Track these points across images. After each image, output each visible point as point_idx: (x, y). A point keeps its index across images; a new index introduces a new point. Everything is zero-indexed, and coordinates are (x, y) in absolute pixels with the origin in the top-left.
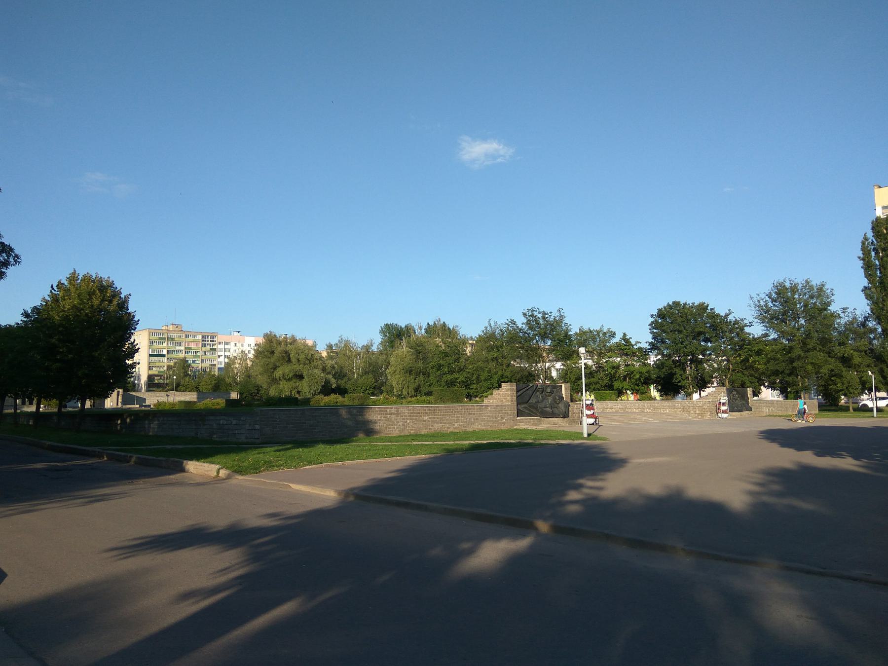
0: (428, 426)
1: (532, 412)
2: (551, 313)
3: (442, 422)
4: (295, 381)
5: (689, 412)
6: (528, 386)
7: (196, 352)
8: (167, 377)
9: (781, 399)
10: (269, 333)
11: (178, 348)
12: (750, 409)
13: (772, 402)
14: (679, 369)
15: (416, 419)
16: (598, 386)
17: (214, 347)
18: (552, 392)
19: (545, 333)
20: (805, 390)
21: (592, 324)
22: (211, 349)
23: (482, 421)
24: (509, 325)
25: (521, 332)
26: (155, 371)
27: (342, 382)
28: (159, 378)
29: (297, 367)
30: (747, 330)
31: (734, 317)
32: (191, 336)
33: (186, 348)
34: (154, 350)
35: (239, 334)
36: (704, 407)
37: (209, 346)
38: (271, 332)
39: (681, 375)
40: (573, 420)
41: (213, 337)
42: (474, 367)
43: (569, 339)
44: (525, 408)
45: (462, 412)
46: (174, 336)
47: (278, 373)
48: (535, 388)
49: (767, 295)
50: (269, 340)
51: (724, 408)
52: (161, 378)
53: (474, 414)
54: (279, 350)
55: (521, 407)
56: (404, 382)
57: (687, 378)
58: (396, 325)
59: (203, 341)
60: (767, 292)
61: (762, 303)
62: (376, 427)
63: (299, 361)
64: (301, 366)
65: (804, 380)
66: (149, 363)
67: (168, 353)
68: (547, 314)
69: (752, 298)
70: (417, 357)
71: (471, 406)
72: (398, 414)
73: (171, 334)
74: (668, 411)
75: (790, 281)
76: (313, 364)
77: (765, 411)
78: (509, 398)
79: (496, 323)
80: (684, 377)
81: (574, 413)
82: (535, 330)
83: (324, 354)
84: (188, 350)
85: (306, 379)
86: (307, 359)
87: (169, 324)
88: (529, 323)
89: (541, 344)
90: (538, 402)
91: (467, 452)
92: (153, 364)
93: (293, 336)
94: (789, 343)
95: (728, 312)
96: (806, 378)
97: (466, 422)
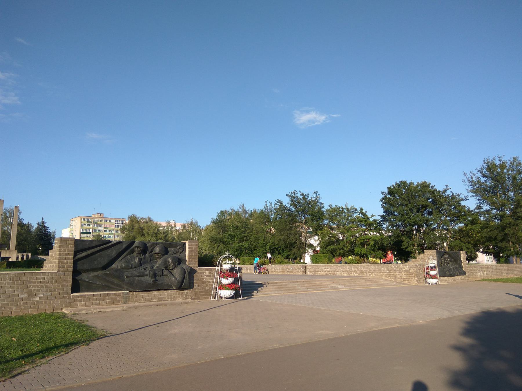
1: (112, 283)
2: (308, 194)
5: (396, 276)
9: (494, 262)
11: (100, 228)
12: (464, 273)
13: (487, 266)
14: (406, 237)
16: (342, 251)
20: (517, 254)
21: (340, 203)
30: (463, 203)
31: (451, 192)
33: (104, 228)
34: (84, 229)
36: (411, 271)
38: (133, 215)
39: (408, 242)
40: (202, 292)
46: (97, 221)
49: (479, 171)
51: (432, 273)
54: (137, 226)
57: (413, 245)
59: (116, 224)
60: (479, 168)
61: (475, 179)
63: (148, 234)
65: (516, 246)
66: (80, 237)
67: (93, 231)
68: (306, 196)
69: (465, 174)
74: (374, 275)
75: (499, 158)
76: (158, 237)
77: (480, 275)
80: (410, 244)
81: (204, 282)
84: (106, 230)
87: (96, 214)
94: (500, 213)
95: (445, 187)
96: (517, 244)
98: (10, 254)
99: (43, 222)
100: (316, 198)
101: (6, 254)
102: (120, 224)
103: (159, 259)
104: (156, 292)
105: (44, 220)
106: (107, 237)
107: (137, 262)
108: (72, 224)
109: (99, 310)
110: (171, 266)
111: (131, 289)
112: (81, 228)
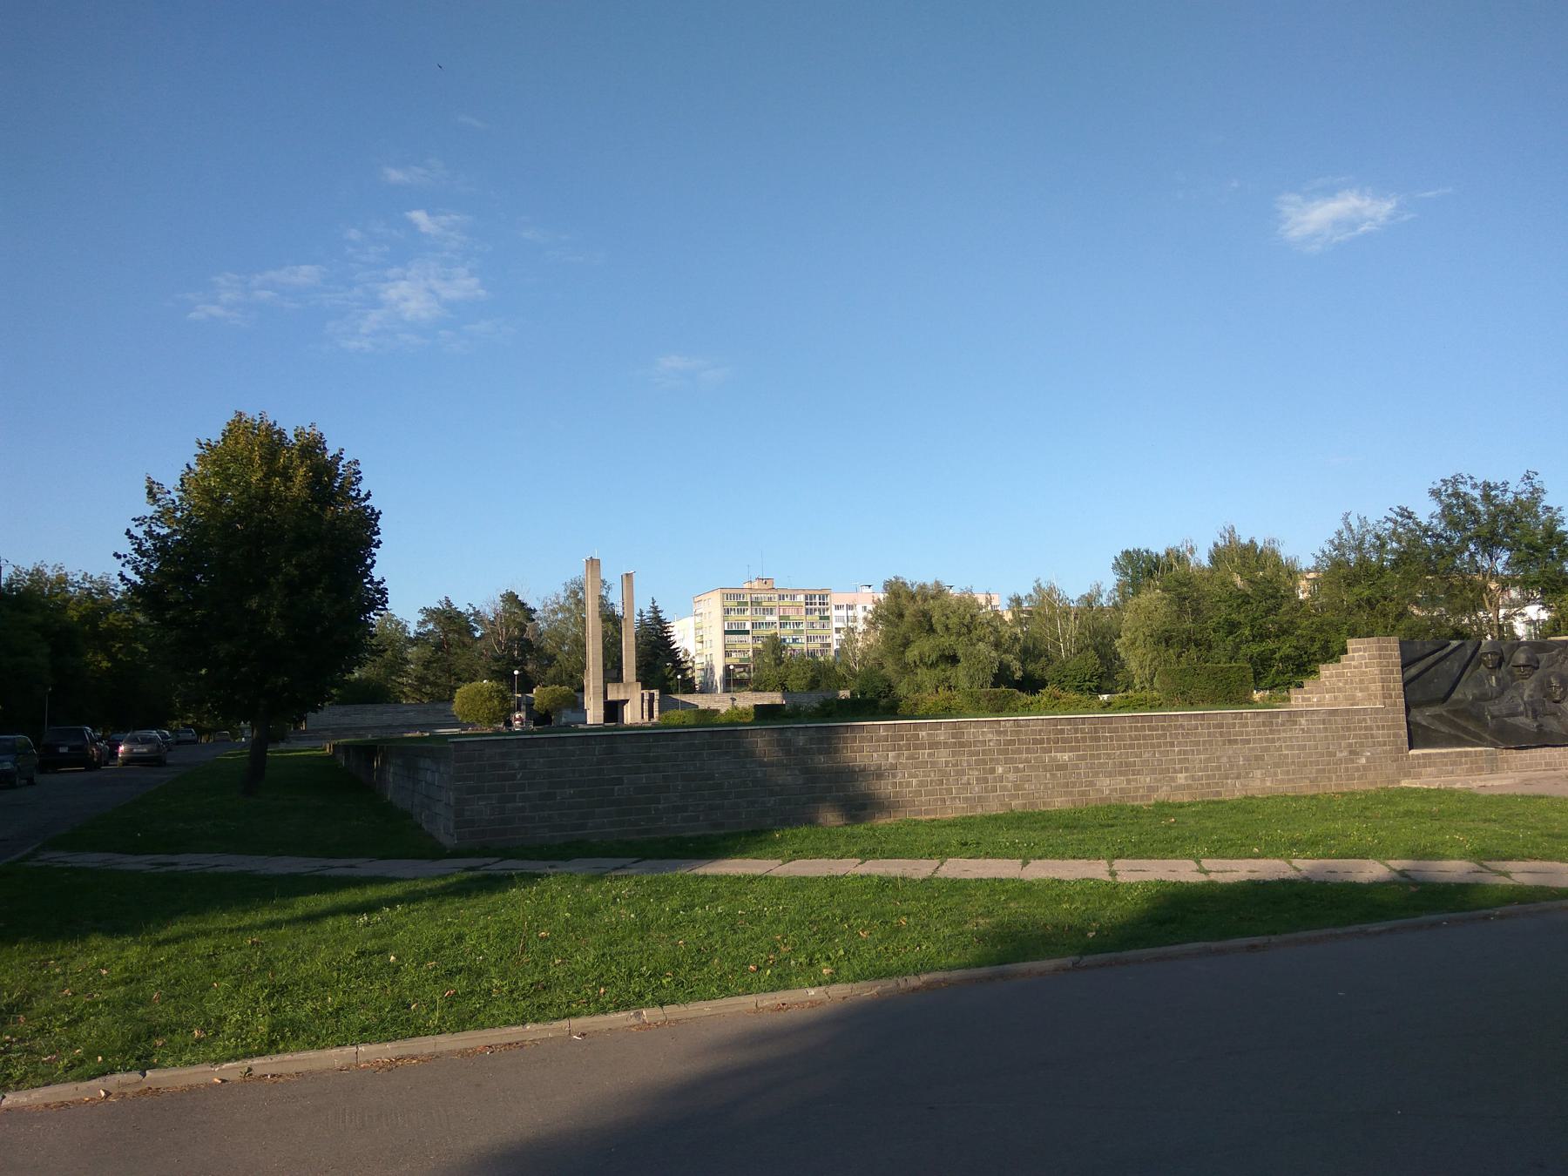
0: (1074, 784)
1: (1465, 730)
2: (1505, 484)
3: (1125, 768)
4: (944, 667)
6: (1443, 648)
7: (798, 624)
8: (754, 668)
10: (893, 579)
11: (769, 618)
15: (1027, 761)
17: (826, 614)
18: (1533, 665)
19: (1493, 533)
22: (821, 618)
23: (1276, 765)
24: (1395, 522)
25: (1430, 536)
26: (735, 659)
27: (1033, 667)
28: (742, 669)
29: (946, 641)
32: (787, 596)
35: (870, 590)
37: (817, 613)
38: (897, 578)
41: (823, 597)
42: (1312, 623)
43: (1559, 544)
44: (1438, 717)
45: (1200, 735)
47: (912, 654)
48: (1469, 652)
50: (894, 593)
52: (744, 671)
53: (1248, 742)
55: (1422, 716)
56: (1156, 663)
58: (1147, 552)
59: (807, 604)
62: (885, 788)
63: (947, 628)
64: (953, 638)
67: (753, 627)
68: (1496, 488)
70: (1182, 610)
71: (1244, 720)
72: (962, 745)
73: (756, 596)
76: (974, 635)
78: (1376, 687)
79: (1363, 521)
82: (1465, 529)
83: (1008, 616)
85: (963, 664)
86: (963, 624)
88: (1447, 510)
89: (1484, 563)
90: (1483, 698)
91: (1088, 959)
92: (730, 647)
93: (937, 582)
97: (1219, 768)
98: (626, 692)
99: (655, 610)
100: (1532, 493)
101: (618, 692)
102: (818, 606)
103: (1526, 679)
104: (1539, 750)
105: (656, 605)
106: (788, 641)
107: (1494, 685)
108: (698, 612)
109: (1483, 784)
110: (1558, 693)
111: (1499, 743)
112: (724, 621)
